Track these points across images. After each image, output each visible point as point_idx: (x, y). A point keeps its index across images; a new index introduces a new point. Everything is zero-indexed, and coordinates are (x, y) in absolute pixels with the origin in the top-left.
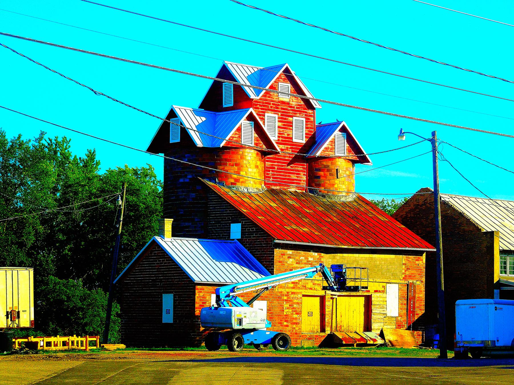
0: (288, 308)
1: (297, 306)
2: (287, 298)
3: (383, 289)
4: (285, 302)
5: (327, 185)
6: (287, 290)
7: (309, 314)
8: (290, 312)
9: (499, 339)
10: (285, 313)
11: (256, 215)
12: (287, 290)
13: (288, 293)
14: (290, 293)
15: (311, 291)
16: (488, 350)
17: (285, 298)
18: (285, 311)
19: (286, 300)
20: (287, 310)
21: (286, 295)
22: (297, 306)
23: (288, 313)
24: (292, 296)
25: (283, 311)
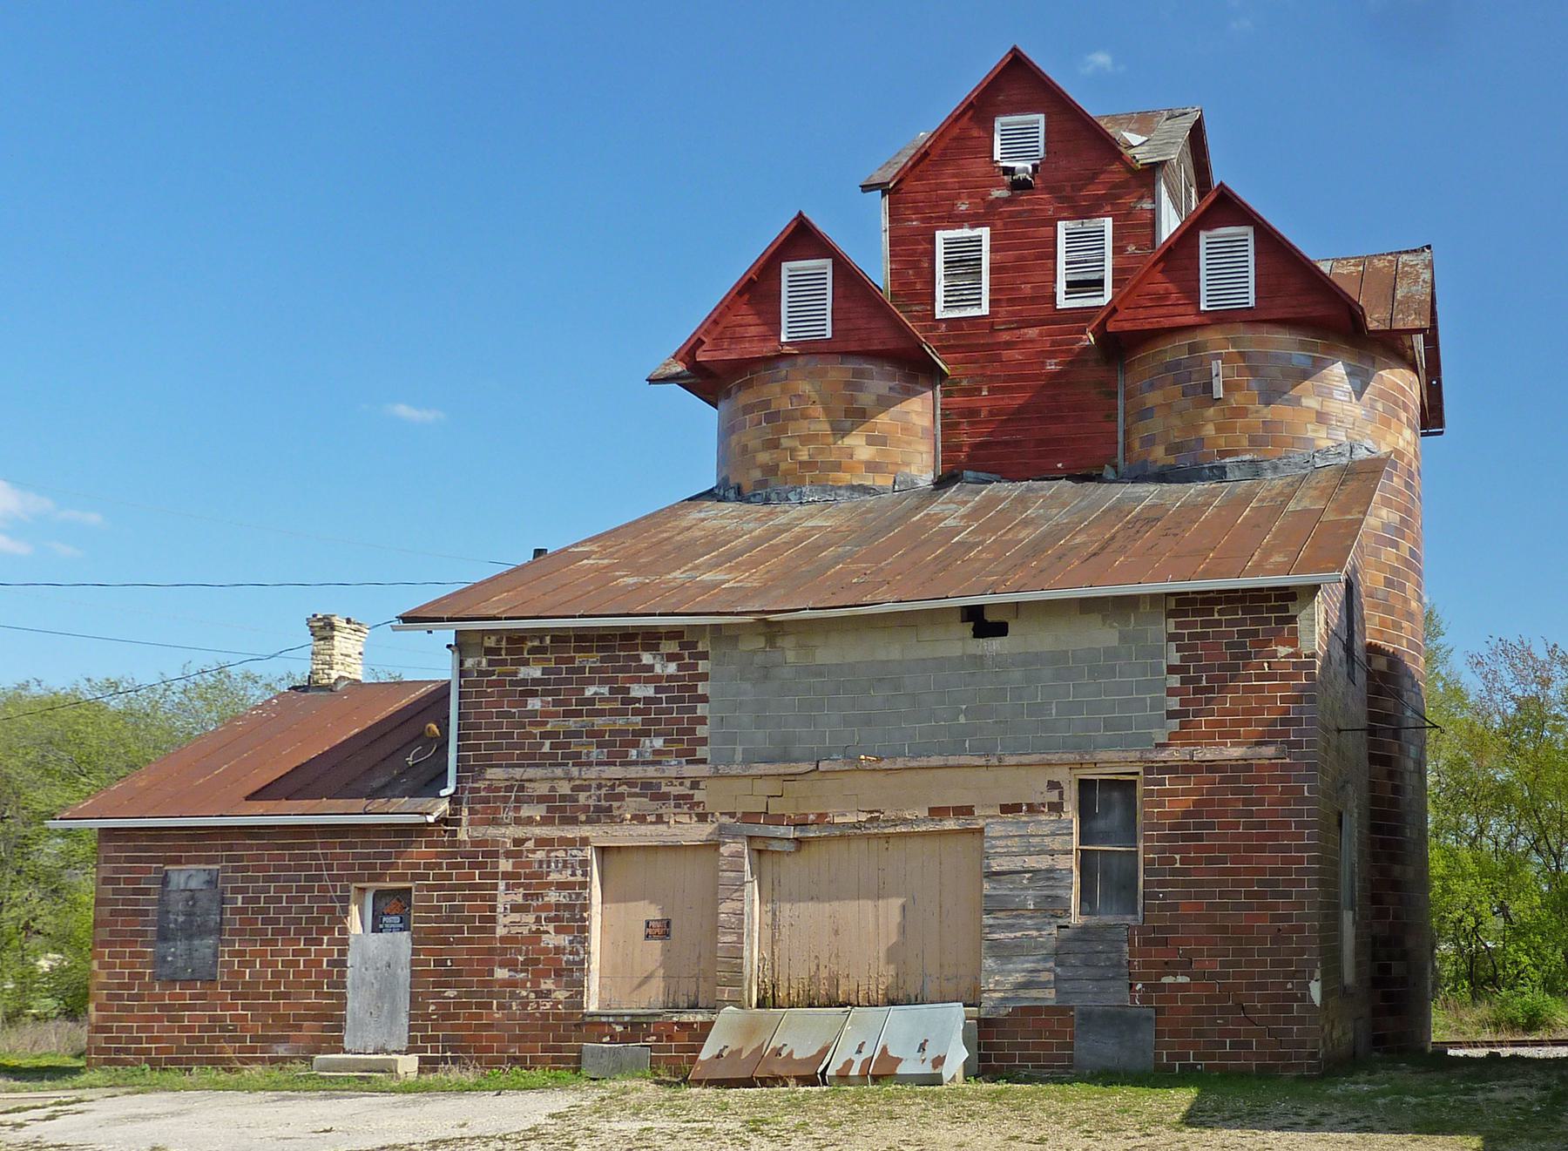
0: (516, 908)
1: (561, 898)
2: (514, 864)
3: (1053, 796)
4: (502, 885)
5: (1176, 434)
6: (520, 832)
7: (649, 930)
8: (526, 924)
9: (163, 671)
10: (500, 931)
11: (1109, 745)
12: (520, 832)
13: (518, 842)
14: (530, 844)
15: (643, 829)
16: (380, 988)
17: (505, 865)
18: (501, 920)
19: (506, 875)
20: (515, 917)
21: (508, 855)
22: (561, 898)
23: (514, 930)
24: (540, 855)
25: (493, 919)
